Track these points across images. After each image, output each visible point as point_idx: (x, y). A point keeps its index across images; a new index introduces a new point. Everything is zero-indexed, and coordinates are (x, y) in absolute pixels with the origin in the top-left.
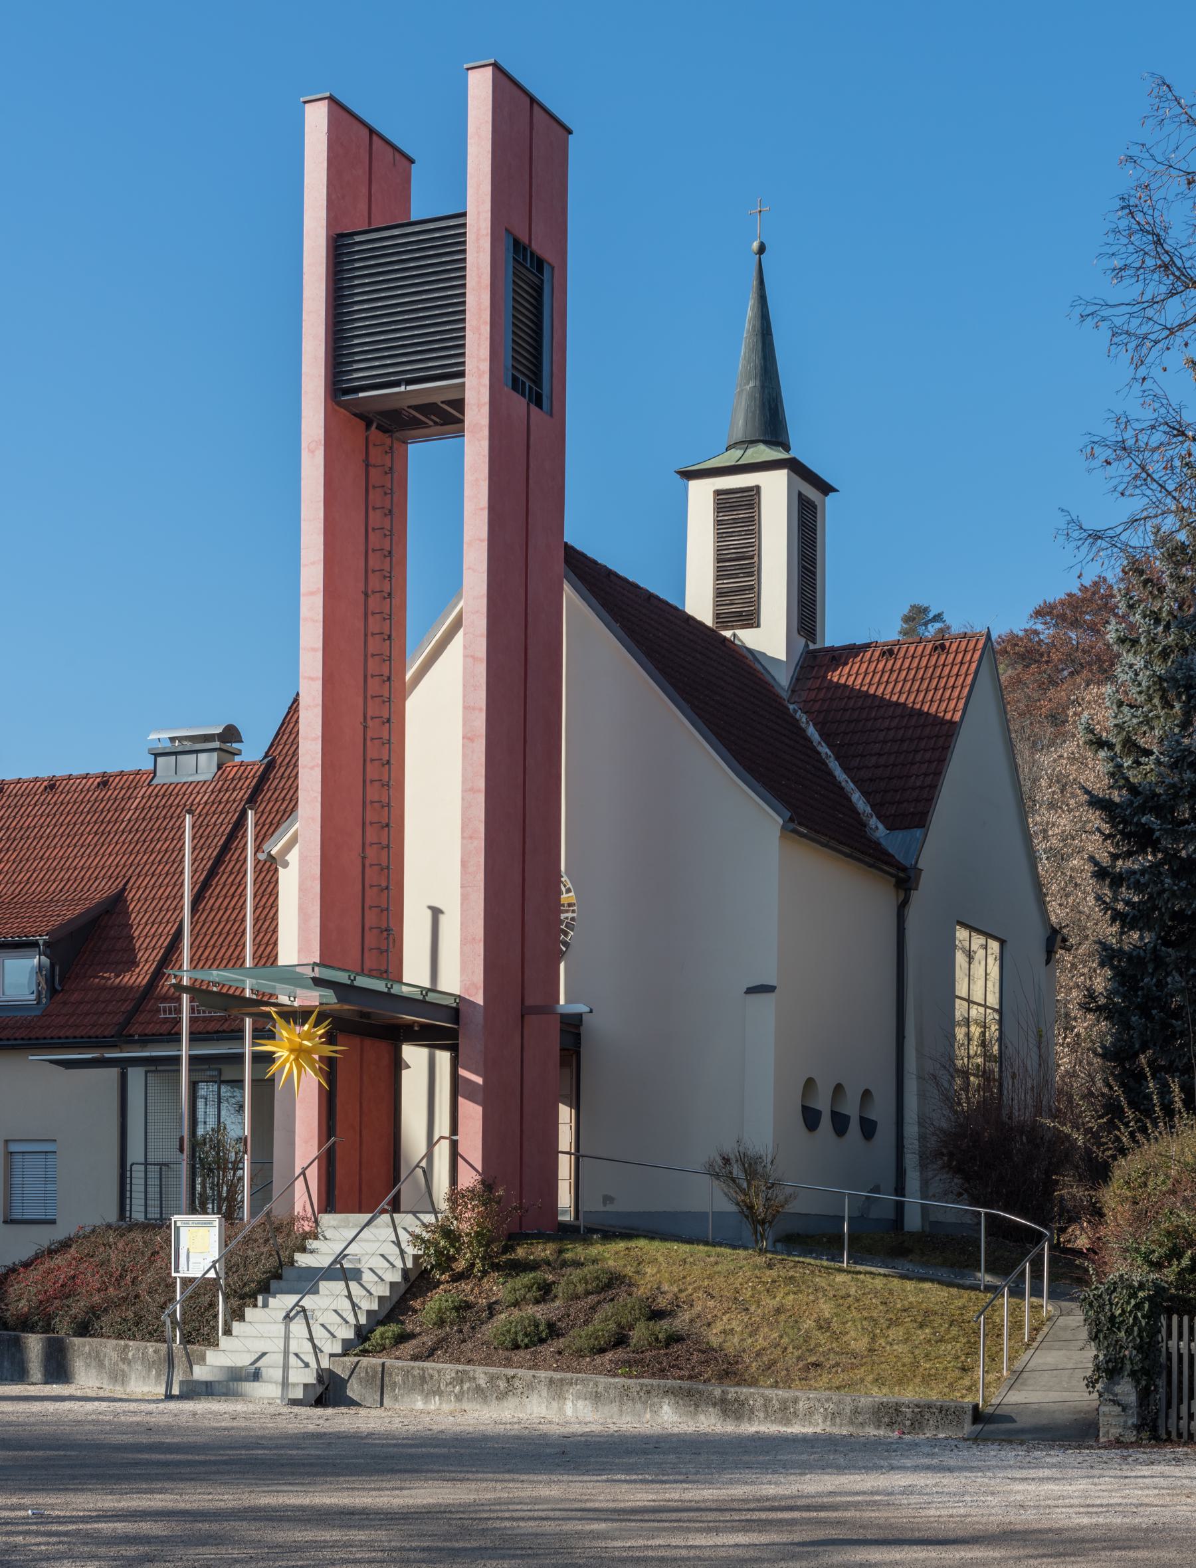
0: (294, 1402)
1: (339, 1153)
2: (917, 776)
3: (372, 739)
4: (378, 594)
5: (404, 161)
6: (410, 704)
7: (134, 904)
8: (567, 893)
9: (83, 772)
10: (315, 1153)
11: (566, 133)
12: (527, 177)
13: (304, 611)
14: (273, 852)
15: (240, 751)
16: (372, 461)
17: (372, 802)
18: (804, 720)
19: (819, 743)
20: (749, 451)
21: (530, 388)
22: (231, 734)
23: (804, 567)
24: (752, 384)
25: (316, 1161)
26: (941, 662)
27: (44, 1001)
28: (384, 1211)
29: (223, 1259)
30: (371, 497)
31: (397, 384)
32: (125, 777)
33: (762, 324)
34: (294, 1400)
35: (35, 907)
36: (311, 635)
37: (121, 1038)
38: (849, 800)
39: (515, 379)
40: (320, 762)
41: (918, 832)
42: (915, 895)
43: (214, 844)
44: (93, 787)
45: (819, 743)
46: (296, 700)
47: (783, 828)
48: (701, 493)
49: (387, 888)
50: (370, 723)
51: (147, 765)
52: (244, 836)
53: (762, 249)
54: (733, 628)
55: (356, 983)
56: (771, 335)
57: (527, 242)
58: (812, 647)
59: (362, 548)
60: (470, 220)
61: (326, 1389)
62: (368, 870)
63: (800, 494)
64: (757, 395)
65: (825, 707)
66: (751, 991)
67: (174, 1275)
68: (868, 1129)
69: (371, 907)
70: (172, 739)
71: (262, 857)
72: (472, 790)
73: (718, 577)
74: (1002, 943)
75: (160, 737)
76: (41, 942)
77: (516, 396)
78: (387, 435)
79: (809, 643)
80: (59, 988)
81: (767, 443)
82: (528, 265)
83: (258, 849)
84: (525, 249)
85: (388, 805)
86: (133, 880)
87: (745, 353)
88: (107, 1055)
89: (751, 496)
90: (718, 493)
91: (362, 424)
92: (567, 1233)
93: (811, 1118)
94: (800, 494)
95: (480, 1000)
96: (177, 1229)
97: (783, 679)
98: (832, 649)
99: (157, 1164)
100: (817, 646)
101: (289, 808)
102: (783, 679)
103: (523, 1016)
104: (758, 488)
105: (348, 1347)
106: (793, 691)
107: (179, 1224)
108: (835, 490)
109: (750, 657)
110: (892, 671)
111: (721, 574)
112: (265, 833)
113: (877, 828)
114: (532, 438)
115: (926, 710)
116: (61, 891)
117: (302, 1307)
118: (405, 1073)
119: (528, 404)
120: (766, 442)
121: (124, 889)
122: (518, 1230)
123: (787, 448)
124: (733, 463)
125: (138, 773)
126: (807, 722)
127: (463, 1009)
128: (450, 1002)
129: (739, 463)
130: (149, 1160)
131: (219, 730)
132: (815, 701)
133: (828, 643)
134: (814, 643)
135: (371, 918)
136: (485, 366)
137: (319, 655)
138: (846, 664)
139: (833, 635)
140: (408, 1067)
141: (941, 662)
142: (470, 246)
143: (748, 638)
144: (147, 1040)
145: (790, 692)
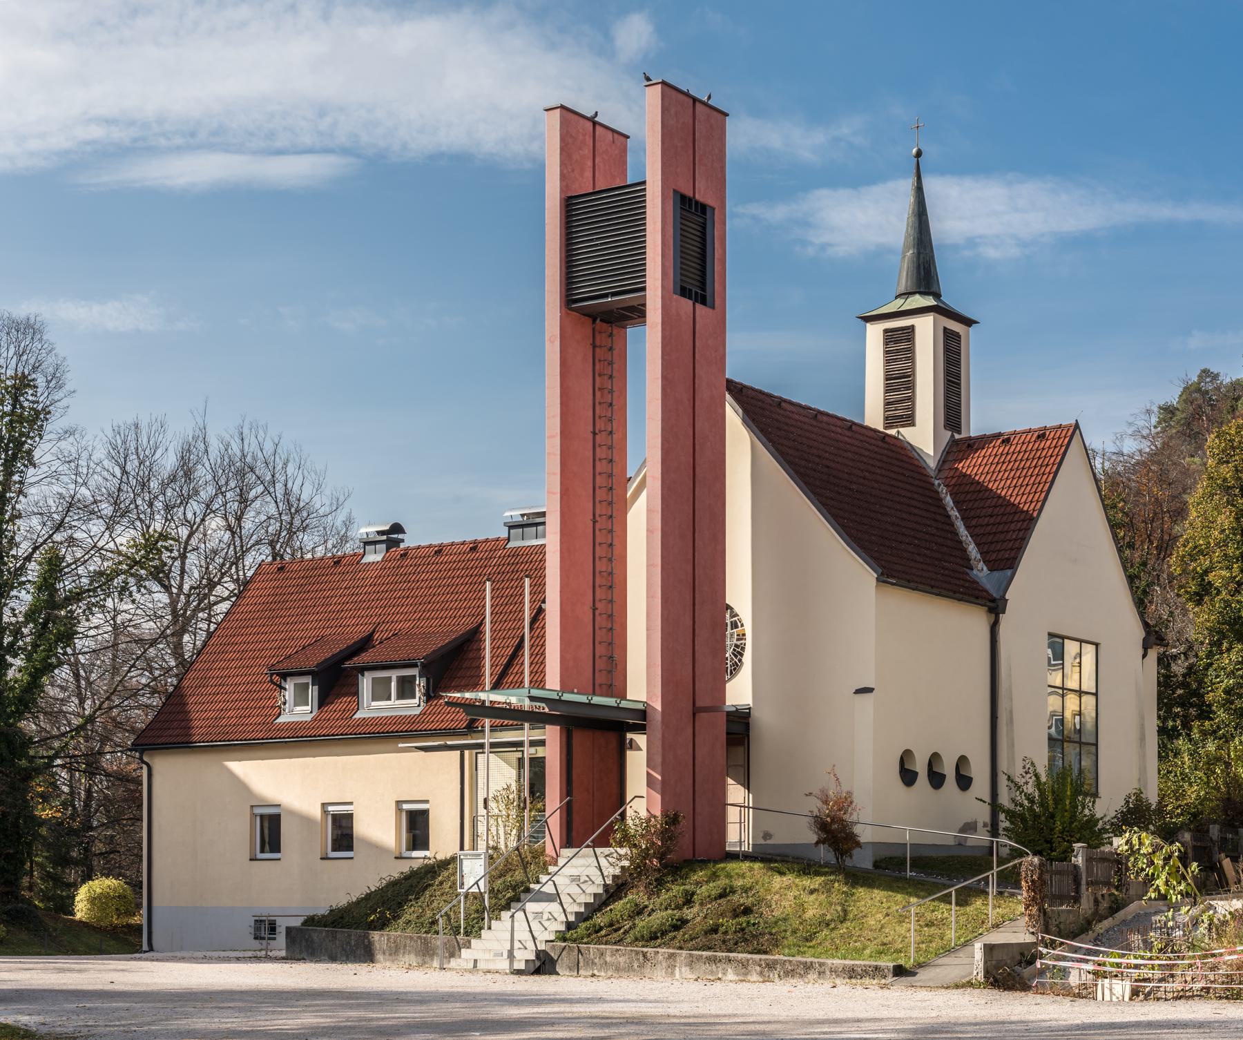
0: (519, 972)
1: (575, 807)
2: (1014, 531)
5: (622, 139)
9: (461, 540)
11: (722, 116)
16: (598, 343)
17: (600, 572)
18: (944, 491)
19: (952, 508)
21: (696, 293)
24: (911, 252)
27: (422, 704)
28: (588, 846)
29: (487, 876)
30: (597, 367)
31: (606, 296)
33: (919, 208)
34: (518, 970)
38: (965, 550)
41: (1009, 572)
42: (1003, 618)
45: (952, 508)
47: (878, 579)
48: (874, 334)
53: (919, 154)
54: (897, 427)
55: (563, 698)
57: (692, 196)
58: (957, 436)
59: (590, 403)
60: (648, 186)
61: (544, 963)
62: (598, 619)
63: (945, 329)
64: (915, 259)
65: (959, 482)
66: (858, 691)
67: (459, 890)
70: (523, 515)
73: (886, 391)
74: (1097, 645)
76: (419, 664)
80: (432, 695)
82: (693, 211)
84: (690, 200)
88: (449, 743)
90: (886, 331)
91: (589, 321)
92: (733, 857)
93: (908, 777)
94: (945, 329)
95: (658, 706)
97: (932, 464)
98: (970, 438)
100: (963, 435)
102: (932, 464)
103: (694, 714)
104: (912, 327)
105: (562, 937)
106: (940, 471)
107: (462, 857)
108: (976, 322)
111: (888, 389)
113: (982, 569)
119: (694, 304)
120: (921, 293)
122: (691, 857)
123: (937, 296)
125: (497, 540)
126: (946, 493)
127: (648, 711)
128: (640, 706)
131: (387, 528)
132: (953, 477)
133: (973, 434)
134: (959, 432)
135: (600, 650)
138: (984, 448)
139: (977, 423)
143: (907, 434)
145: (937, 471)
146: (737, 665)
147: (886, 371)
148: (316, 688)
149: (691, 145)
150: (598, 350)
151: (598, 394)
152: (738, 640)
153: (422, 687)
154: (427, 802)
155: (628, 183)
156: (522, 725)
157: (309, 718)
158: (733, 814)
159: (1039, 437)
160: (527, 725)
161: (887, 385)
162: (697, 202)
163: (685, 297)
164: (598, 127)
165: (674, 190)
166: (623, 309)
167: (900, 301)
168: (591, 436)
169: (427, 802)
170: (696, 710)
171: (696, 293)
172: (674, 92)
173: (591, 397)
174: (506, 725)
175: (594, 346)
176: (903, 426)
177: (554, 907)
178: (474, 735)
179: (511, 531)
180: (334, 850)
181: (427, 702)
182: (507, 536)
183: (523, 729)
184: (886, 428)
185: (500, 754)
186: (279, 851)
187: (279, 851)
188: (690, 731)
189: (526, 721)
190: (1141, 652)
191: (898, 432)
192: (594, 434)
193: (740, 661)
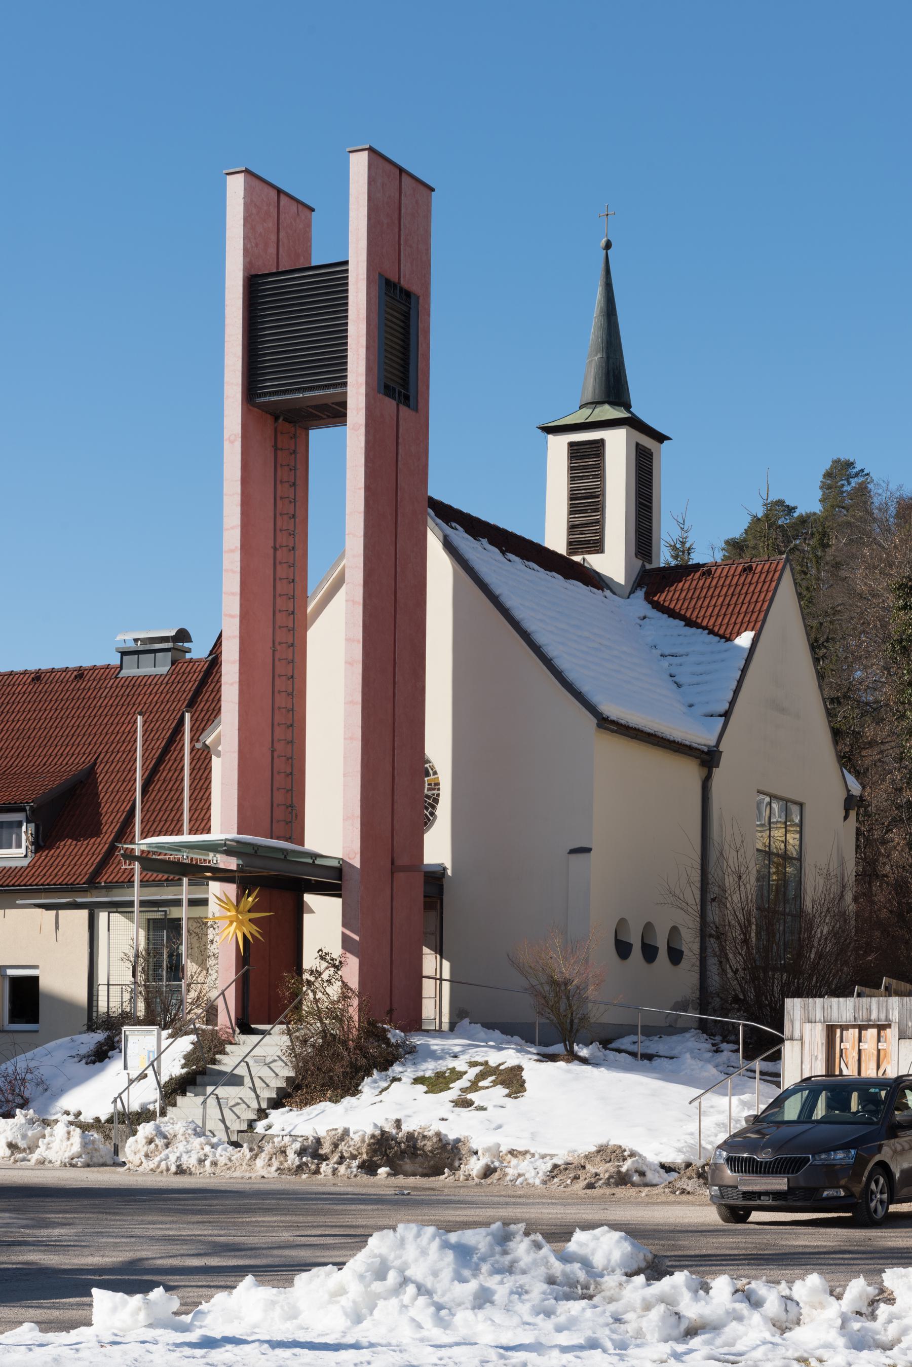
3: (280, 660)
4: (284, 548)
6: (311, 634)
7: (102, 775)
8: (433, 775)
10: (234, 977)
12: (397, 230)
13: (226, 564)
14: (207, 743)
15: (190, 649)
16: (280, 445)
20: (597, 410)
21: (400, 392)
22: (183, 636)
23: (641, 503)
24: (599, 356)
25: (234, 983)
26: (748, 580)
27: (29, 854)
32: (97, 671)
35: (23, 778)
36: (231, 583)
37: (92, 883)
39: (387, 387)
40: (238, 680)
42: (716, 771)
43: (167, 727)
44: (70, 679)
46: (220, 636)
48: (558, 445)
49: (291, 774)
50: (278, 647)
51: (115, 660)
52: (182, 739)
53: (608, 245)
54: (582, 553)
56: (616, 315)
57: (396, 281)
58: (648, 566)
59: (272, 514)
60: (351, 267)
62: (276, 761)
63: (637, 444)
64: (604, 365)
66: (573, 851)
68: (675, 956)
69: (278, 789)
70: (136, 640)
71: (198, 745)
72: (352, 702)
73: (571, 512)
75: (127, 638)
76: (28, 808)
77: (387, 400)
78: (292, 425)
79: (645, 563)
80: (42, 844)
81: (613, 404)
83: (194, 739)
85: (292, 710)
86: (102, 756)
87: (594, 330)
88: (79, 900)
89: (600, 445)
90: (571, 445)
91: (270, 420)
93: (623, 949)
94: (637, 444)
95: (356, 862)
96: (126, 1037)
99: (119, 985)
100: (654, 566)
101: (215, 711)
103: (392, 873)
104: (602, 442)
108: (668, 438)
109: (597, 577)
110: (709, 587)
112: (198, 731)
114: (401, 431)
115: (716, 631)
116: (45, 764)
117: (216, 1095)
118: (307, 917)
119: (398, 405)
121: (95, 764)
123: (627, 406)
124: (583, 421)
127: (345, 869)
128: (335, 864)
129: (587, 421)
130: (111, 982)
131: (173, 633)
135: (279, 797)
136: (362, 379)
137: (237, 599)
140: (312, 911)
141: (748, 580)
142: (351, 288)
144: (110, 887)
146: (429, 820)
147: (571, 490)
148: (32, 827)
149: (397, 222)
150: (279, 453)
151: (279, 503)
152: (429, 790)
153: (30, 835)
154: (35, 967)
155: (313, 264)
156: (180, 880)
157: (25, 863)
158: (428, 987)
159: (744, 570)
160: (185, 880)
161: (571, 506)
162: (402, 289)
163: (389, 396)
164: (282, 196)
165: (379, 273)
166: (311, 407)
167: (586, 412)
168: (272, 551)
169: (35, 967)
170: (394, 869)
171: (400, 392)
172: (381, 160)
173: (271, 507)
174: (172, 880)
175: (276, 449)
176: (589, 553)
177: (244, 1092)
178: (95, 892)
179: (124, 657)
180: (12, 1021)
181: (36, 853)
182: (119, 663)
183: (181, 885)
184: (570, 554)
185: (127, 914)
186: (35, 1020)
187: (35, 1020)
188: (388, 892)
189: (184, 875)
190: (843, 813)
191: (584, 559)
192: (275, 549)
193: (432, 814)
